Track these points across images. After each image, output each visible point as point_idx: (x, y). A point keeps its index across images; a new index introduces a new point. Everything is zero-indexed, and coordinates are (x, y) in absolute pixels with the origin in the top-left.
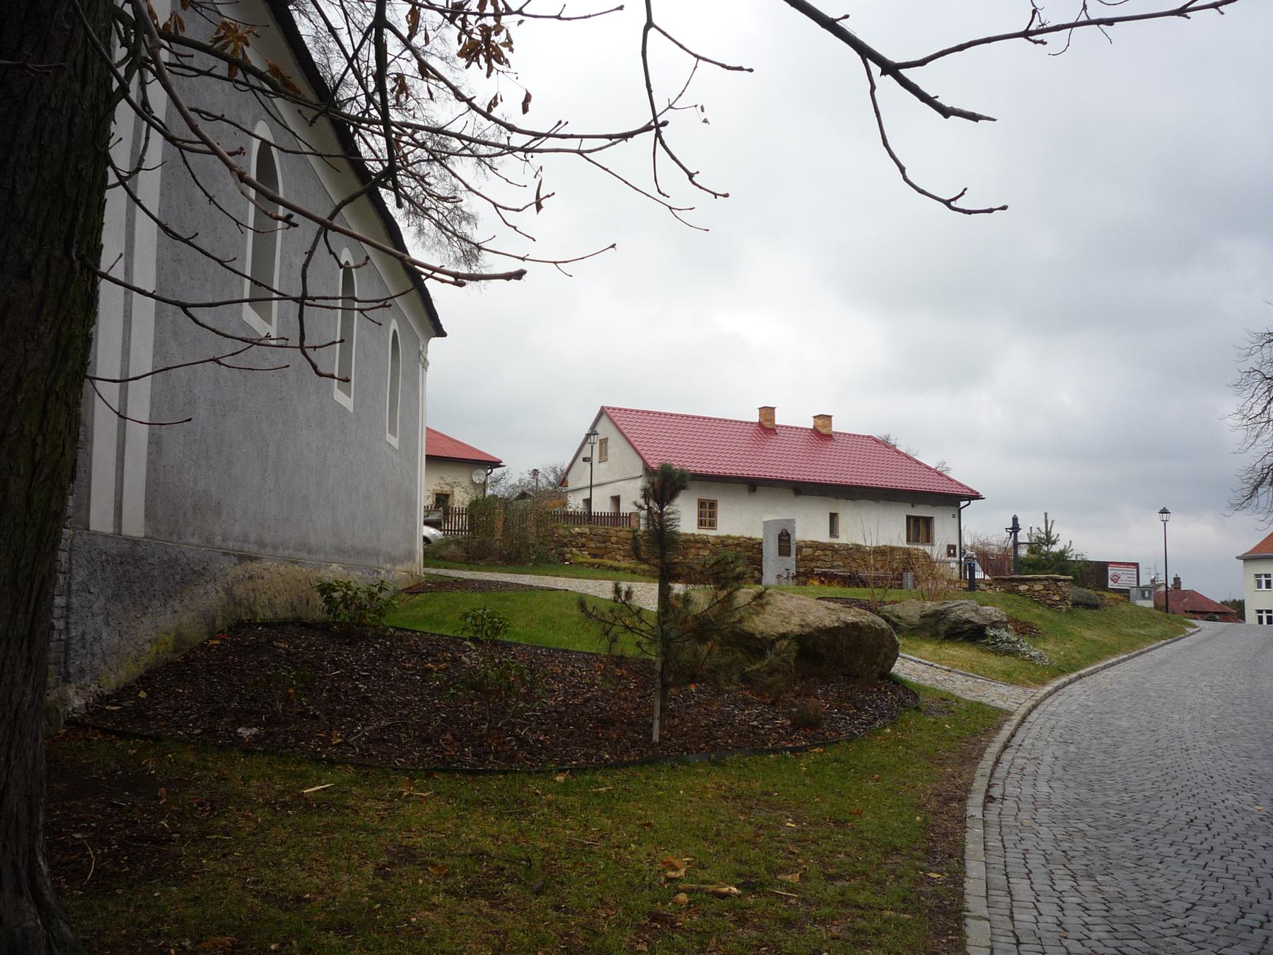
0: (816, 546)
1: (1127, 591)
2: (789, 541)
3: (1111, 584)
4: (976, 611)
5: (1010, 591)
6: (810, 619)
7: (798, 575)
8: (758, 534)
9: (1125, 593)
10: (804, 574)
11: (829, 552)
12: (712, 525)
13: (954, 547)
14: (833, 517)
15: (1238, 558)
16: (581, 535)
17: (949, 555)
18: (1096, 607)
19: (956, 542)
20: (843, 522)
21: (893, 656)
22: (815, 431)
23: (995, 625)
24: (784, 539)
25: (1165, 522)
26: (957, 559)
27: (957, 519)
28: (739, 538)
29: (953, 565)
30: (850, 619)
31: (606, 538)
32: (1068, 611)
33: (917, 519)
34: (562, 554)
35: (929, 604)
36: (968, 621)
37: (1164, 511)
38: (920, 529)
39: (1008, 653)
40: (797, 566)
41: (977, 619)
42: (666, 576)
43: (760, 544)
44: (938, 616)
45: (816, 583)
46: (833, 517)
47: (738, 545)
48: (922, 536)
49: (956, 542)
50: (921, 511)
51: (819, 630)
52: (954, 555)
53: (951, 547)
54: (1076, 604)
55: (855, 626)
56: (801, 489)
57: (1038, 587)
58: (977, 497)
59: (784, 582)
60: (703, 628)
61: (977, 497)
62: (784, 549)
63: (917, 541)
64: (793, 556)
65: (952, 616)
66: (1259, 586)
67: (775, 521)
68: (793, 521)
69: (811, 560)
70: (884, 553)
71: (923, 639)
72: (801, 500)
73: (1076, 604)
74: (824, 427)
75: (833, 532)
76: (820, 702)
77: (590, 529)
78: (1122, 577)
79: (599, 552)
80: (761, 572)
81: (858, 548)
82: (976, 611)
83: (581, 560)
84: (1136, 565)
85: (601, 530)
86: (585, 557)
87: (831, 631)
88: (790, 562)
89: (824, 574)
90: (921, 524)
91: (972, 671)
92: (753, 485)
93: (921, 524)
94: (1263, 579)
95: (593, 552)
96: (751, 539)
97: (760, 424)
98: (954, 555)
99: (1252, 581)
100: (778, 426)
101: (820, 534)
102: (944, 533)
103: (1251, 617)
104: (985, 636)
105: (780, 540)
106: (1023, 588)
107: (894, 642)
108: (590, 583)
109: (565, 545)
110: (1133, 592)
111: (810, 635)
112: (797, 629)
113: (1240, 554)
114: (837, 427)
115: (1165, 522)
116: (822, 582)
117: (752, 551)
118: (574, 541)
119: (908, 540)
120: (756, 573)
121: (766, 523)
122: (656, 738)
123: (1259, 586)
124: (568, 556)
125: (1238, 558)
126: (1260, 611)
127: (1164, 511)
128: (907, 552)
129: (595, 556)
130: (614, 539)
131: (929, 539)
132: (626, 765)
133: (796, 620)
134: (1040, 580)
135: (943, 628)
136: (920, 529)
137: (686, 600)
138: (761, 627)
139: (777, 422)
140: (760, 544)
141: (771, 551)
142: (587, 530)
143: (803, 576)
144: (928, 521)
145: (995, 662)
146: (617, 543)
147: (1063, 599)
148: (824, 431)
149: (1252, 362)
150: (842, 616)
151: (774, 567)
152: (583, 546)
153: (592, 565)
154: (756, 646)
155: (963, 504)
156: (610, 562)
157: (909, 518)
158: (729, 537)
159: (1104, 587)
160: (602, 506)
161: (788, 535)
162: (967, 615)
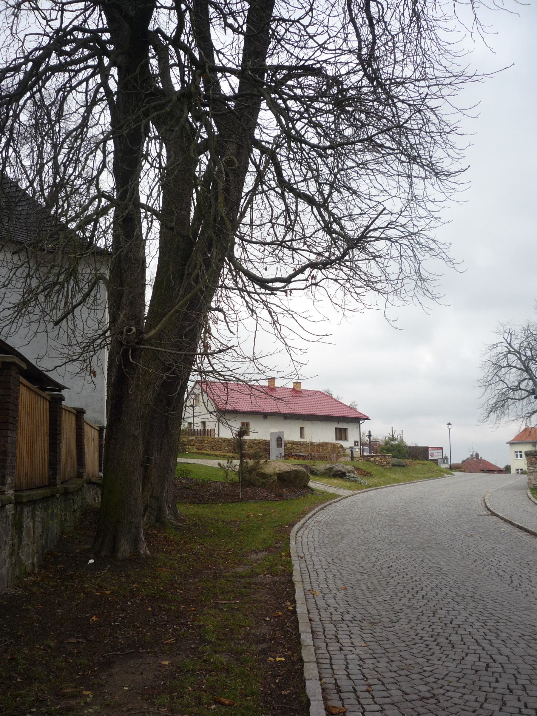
0: (293, 443)
1: (437, 460)
2: (281, 441)
3: (430, 457)
4: (343, 467)
5: (367, 461)
6: (282, 469)
7: (285, 456)
8: (268, 438)
9: (435, 461)
10: (288, 455)
11: (299, 446)
12: (243, 424)
13: (357, 442)
14: (302, 429)
15: (507, 443)
16: (192, 440)
17: (355, 445)
18: (403, 466)
19: (358, 439)
20: (306, 431)
21: (308, 480)
22: (294, 389)
23: (349, 472)
24: (279, 440)
25: (449, 429)
26: (359, 447)
27: (358, 429)
28: (259, 440)
29: (357, 450)
30: (294, 469)
31: (203, 442)
32: (390, 468)
33: (340, 429)
34: (185, 449)
35: (328, 465)
36: (340, 471)
37: (449, 424)
38: (342, 434)
39: (353, 481)
40: (285, 452)
41: (343, 470)
42: (242, 456)
43: (269, 442)
44: (330, 469)
45: (293, 459)
46: (302, 429)
47: (259, 443)
48: (343, 437)
49: (358, 439)
50: (342, 426)
51: (284, 472)
52: (358, 445)
53: (356, 442)
54: (394, 465)
55: (295, 470)
56: (287, 417)
57: (378, 459)
58: (367, 418)
59: (279, 459)
60: (252, 470)
61: (367, 418)
62: (279, 445)
63: (341, 439)
64: (283, 447)
65: (335, 469)
66: (517, 457)
67: (275, 432)
68: (283, 432)
69: (291, 449)
70: (323, 445)
71: (325, 477)
72: (288, 421)
73: (394, 465)
74: (298, 387)
75: (302, 436)
76: (285, 491)
77: (196, 438)
78: (436, 454)
79: (200, 448)
80: (269, 454)
81: (312, 443)
82: (343, 467)
83: (193, 451)
84: (442, 448)
85: (200, 438)
86: (194, 450)
87: (288, 472)
88: (282, 450)
89: (296, 455)
90: (343, 432)
91: (338, 486)
92: (266, 415)
93: (343, 432)
94: (519, 454)
95: (198, 447)
96: (265, 440)
97: (268, 386)
98: (358, 445)
99: (514, 455)
100: (276, 387)
101: (296, 438)
102: (353, 436)
103: (513, 471)
104: (346, 476)
105: (277, 441)
106: (372, 459)
107: (309, 477)
108: (201, 460)
109: (186, 445)
110: (439, 460)
111: (282, 473)
112: (278, 472)
113: (508, 441)
114: (304, 387)
115: (449, 429)
116: (295, 459)
117: (265, 446)
118: (190, 443)
119: (336, 439)
120: (267, 455)
121: (271, 433)
122: (241, 497)
123: (517, 457)
124: (187, 450)
125: (507, 443)
126: (518, 470)
127: (449, 424)
128: (334, 446)
129: (198, 449)
130: (206, 442)
131: (346, 439)
132: (234, 502)
133: (277, 469)
134: (379, 456)
135: (332, 473)
136: (342, 434)
137: (247, 463)
138: (267, 471)
139: (276, 386)
140: (269, 442)
141: (273, 445)
142: (194, 438)
143: (287, 456)
144: (345, 430)
145: (348, 484)
146: (208, 443)
147: (388, 463)
148: (298, 389)
149: (487, 357)
150: (292, 468)
151: (275, 451)
152: (193, 445)
153: (198, 453)
154: (264, 476)
155: (361, 422)
156: (206, 452)
157: (336, 429)
158: (255, 440)
159: (427, 459)
160: (198, 427)
161: (281, 438)
162: (340, 469)
